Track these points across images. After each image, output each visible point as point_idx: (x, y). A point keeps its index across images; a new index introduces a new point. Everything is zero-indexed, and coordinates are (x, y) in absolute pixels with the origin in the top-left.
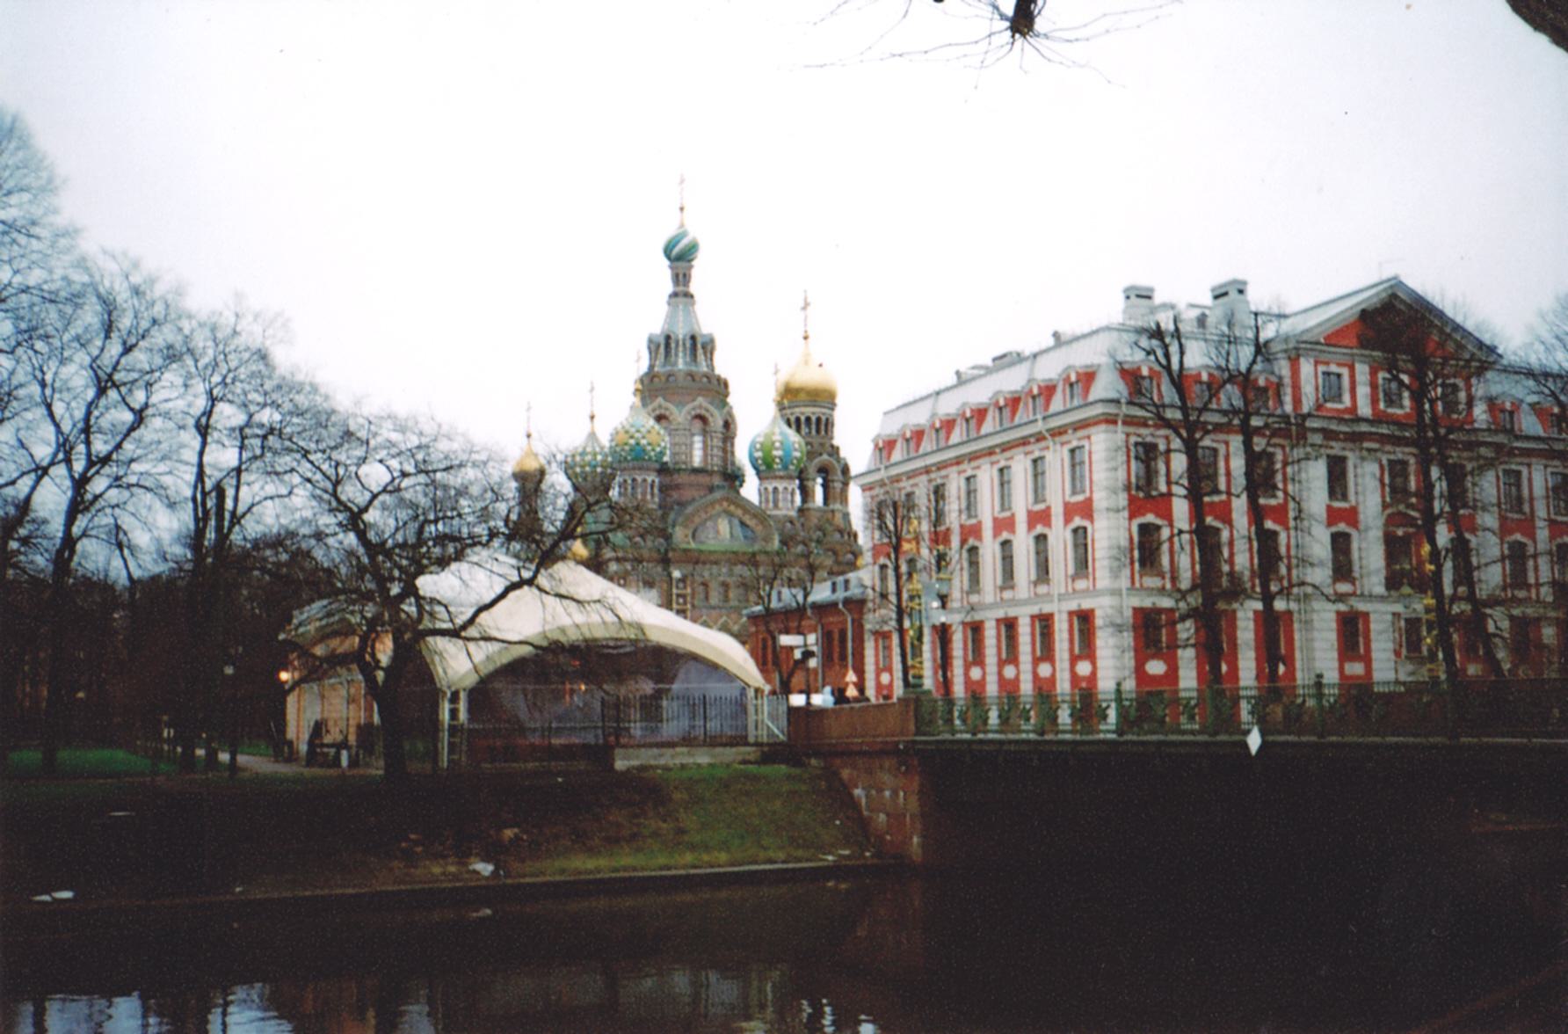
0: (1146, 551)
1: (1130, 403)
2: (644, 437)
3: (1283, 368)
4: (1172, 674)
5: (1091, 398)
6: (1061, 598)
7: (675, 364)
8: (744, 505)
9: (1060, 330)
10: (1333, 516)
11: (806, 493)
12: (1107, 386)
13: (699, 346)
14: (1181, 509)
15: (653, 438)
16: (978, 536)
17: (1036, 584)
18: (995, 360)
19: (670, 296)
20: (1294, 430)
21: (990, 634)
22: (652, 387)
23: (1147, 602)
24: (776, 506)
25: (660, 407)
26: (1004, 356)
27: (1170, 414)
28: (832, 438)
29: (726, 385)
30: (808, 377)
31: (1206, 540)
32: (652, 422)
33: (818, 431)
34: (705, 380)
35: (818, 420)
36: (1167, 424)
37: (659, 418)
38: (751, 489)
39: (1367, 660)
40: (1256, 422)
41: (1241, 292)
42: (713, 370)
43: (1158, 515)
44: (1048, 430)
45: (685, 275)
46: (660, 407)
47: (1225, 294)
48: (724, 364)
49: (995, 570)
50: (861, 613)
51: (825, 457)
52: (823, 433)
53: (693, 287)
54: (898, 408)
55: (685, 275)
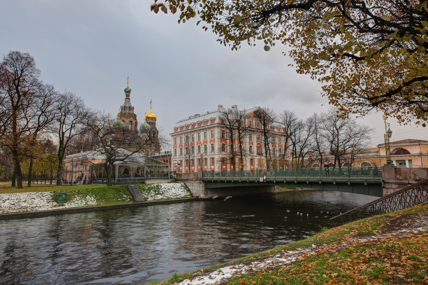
0: (223, 148)
3: (243, 119)
4: (226, 168)
5: (215, 123)
6: (209, 155)
10: (250, 143)
12: (217, 121)
14: (228, 141)
16: (207, 143)
17: (211, 152)
20: (245, 130)
22: (121, 115)
29: (136, 116)
31: (232, 146)
35: (151, 123)
36: (227, 128)
39: (254, 166)
43: (225, 142)
50: (171, 157)
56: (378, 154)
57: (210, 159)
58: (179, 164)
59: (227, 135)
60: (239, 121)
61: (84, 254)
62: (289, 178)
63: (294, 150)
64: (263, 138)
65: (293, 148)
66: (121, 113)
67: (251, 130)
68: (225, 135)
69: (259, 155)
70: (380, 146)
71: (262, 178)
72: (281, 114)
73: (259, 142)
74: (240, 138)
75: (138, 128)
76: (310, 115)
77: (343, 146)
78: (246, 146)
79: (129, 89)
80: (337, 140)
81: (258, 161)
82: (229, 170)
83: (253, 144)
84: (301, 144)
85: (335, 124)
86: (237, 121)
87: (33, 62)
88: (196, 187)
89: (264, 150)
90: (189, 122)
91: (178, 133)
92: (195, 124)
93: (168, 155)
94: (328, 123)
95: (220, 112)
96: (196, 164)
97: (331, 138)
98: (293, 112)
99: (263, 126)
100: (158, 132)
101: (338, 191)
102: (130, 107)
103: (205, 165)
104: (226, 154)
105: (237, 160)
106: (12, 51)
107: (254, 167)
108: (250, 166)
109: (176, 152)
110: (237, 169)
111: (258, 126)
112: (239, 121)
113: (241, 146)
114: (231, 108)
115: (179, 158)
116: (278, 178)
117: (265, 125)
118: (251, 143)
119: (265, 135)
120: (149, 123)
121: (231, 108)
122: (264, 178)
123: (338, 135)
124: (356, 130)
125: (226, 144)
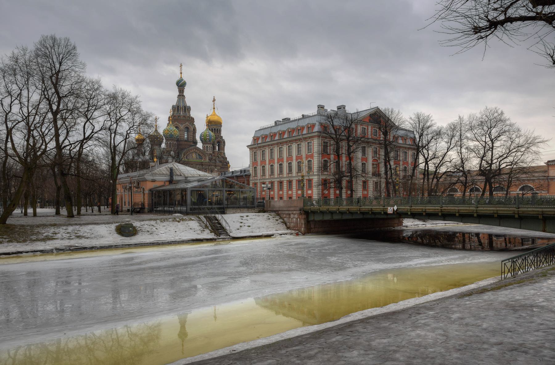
0: (324, 167)
1: (323, 133)
5: (314, 131)
7: (180, 113)
8: (198, 149)
10: (362, 159)
11: (214, 148)
12: (316, 129)
14: (332, 157)
15: (175, 132)
18: (282, 119)
20: (356, 141)
23: (324, 177)
24: (207, 151)
25: (176, 124)
26: (286, 119)
27: (332, 136)
29: (193, 119)
30: (215, 118)
31: (338, 164)
32: (175, 128)
35: (215, 129)
36: (332, 138)
37: (176, 127)
38: (200, 145)
39: (368, 191)
40: (351, 138)
41: (344, 108)
45: (182, 90)
46: (176, 124)
47: (341, 108)
48: (193, 114)
50: (249, 178)
51: (219, 139)
53: (185, 94)
54: (259, 130)
55: (182, 90)
56: (547, 175)
58: (269, 189)
59: (331, 149)
60: (348, 129)
61: (23, 321)
62: (133, 201)
63: (427, 169)
64: (382, 153)
65: (425, 166)
67: (363, 141)
68: (329, 147)
69: (374, 175)
70: (549, 163)
72: (411, 118)
73: (376, 158)
74: (349, 153)
76: (453, 119)
77: (498, 163)
78: (358, 163)
79: (182, 82)
80: (490, 156)
81: (373, 184)
82: (332, 196)
83: (366, 161)
84: (437, 161)
85: (490, 133)
86: (346, 128)
87: (75, 52)
89: (382, 169)
90: (275, 130)
92: (284, 133)
93: (245, 175)
94: (478, 131)
95: (321, 115)
96: (276, 188)
97: (482, 152)
98: (430, 116)
99: (382, 136)
100: (224, 142)
101: (500, 226)
102: (185, 107)
103: (309, 189)
104: (329, 176)
105: (344, 183)
106: (46, 35)
107: (368, 193)
108: (362, 192)
110: (344, 196)
111: (374, 135)
112: (348, 129)
113: (350, 164)
114: (336, 110)
115: (261, 180)
116: (415, 209)
117: (385, 134)
118: (365, 159)
119: (386, 149)
120: (212, 129)
121: (336, 110)
123: (492, 148)
124: (521, 141)
125: (329, 161)
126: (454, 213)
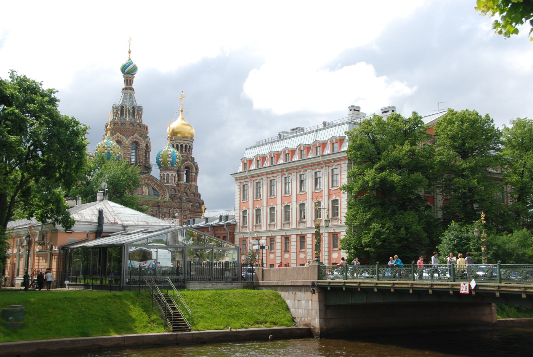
2: (112, 150)
8: (153, 179)
9: (327, 121)
11: (179, 177)
13: (136, 112)
18: (292, 130)
19: (123, 89)
21: (278, 241)
25: (118, 137)
28: (191, 154)
29: (147, 129)
32: (115, 143)
33: (186, 151)
34: (138, 126)
35: (182, 146)
37: (118, 142)
38: (156, 173)
42: (141, 122)
44: (323, 161)
45: (130, 80)
46: (118, 137)
49: (267, 213)
51: (188, 162)
52: (184, 151)
53: (134, 86)
55: (130, 80)
57: (329, 236)
66: (114, 123)
71: (467, 285)
75: (153, 161)
79: (131, 66)
88: (303, 302)
90: (278, 147)
91: (252, 173)
109: (244, 218)
114: (380, 114)
120: (177, 146)
122: (470, 286)
126: (427, 289)
